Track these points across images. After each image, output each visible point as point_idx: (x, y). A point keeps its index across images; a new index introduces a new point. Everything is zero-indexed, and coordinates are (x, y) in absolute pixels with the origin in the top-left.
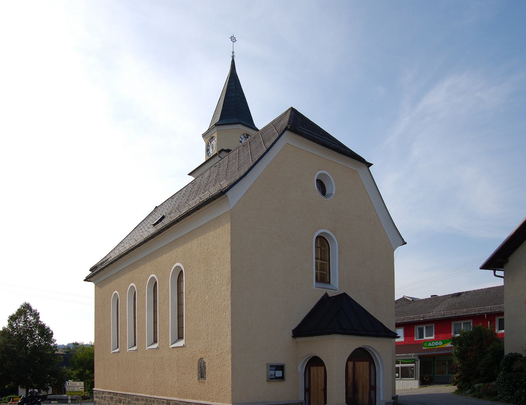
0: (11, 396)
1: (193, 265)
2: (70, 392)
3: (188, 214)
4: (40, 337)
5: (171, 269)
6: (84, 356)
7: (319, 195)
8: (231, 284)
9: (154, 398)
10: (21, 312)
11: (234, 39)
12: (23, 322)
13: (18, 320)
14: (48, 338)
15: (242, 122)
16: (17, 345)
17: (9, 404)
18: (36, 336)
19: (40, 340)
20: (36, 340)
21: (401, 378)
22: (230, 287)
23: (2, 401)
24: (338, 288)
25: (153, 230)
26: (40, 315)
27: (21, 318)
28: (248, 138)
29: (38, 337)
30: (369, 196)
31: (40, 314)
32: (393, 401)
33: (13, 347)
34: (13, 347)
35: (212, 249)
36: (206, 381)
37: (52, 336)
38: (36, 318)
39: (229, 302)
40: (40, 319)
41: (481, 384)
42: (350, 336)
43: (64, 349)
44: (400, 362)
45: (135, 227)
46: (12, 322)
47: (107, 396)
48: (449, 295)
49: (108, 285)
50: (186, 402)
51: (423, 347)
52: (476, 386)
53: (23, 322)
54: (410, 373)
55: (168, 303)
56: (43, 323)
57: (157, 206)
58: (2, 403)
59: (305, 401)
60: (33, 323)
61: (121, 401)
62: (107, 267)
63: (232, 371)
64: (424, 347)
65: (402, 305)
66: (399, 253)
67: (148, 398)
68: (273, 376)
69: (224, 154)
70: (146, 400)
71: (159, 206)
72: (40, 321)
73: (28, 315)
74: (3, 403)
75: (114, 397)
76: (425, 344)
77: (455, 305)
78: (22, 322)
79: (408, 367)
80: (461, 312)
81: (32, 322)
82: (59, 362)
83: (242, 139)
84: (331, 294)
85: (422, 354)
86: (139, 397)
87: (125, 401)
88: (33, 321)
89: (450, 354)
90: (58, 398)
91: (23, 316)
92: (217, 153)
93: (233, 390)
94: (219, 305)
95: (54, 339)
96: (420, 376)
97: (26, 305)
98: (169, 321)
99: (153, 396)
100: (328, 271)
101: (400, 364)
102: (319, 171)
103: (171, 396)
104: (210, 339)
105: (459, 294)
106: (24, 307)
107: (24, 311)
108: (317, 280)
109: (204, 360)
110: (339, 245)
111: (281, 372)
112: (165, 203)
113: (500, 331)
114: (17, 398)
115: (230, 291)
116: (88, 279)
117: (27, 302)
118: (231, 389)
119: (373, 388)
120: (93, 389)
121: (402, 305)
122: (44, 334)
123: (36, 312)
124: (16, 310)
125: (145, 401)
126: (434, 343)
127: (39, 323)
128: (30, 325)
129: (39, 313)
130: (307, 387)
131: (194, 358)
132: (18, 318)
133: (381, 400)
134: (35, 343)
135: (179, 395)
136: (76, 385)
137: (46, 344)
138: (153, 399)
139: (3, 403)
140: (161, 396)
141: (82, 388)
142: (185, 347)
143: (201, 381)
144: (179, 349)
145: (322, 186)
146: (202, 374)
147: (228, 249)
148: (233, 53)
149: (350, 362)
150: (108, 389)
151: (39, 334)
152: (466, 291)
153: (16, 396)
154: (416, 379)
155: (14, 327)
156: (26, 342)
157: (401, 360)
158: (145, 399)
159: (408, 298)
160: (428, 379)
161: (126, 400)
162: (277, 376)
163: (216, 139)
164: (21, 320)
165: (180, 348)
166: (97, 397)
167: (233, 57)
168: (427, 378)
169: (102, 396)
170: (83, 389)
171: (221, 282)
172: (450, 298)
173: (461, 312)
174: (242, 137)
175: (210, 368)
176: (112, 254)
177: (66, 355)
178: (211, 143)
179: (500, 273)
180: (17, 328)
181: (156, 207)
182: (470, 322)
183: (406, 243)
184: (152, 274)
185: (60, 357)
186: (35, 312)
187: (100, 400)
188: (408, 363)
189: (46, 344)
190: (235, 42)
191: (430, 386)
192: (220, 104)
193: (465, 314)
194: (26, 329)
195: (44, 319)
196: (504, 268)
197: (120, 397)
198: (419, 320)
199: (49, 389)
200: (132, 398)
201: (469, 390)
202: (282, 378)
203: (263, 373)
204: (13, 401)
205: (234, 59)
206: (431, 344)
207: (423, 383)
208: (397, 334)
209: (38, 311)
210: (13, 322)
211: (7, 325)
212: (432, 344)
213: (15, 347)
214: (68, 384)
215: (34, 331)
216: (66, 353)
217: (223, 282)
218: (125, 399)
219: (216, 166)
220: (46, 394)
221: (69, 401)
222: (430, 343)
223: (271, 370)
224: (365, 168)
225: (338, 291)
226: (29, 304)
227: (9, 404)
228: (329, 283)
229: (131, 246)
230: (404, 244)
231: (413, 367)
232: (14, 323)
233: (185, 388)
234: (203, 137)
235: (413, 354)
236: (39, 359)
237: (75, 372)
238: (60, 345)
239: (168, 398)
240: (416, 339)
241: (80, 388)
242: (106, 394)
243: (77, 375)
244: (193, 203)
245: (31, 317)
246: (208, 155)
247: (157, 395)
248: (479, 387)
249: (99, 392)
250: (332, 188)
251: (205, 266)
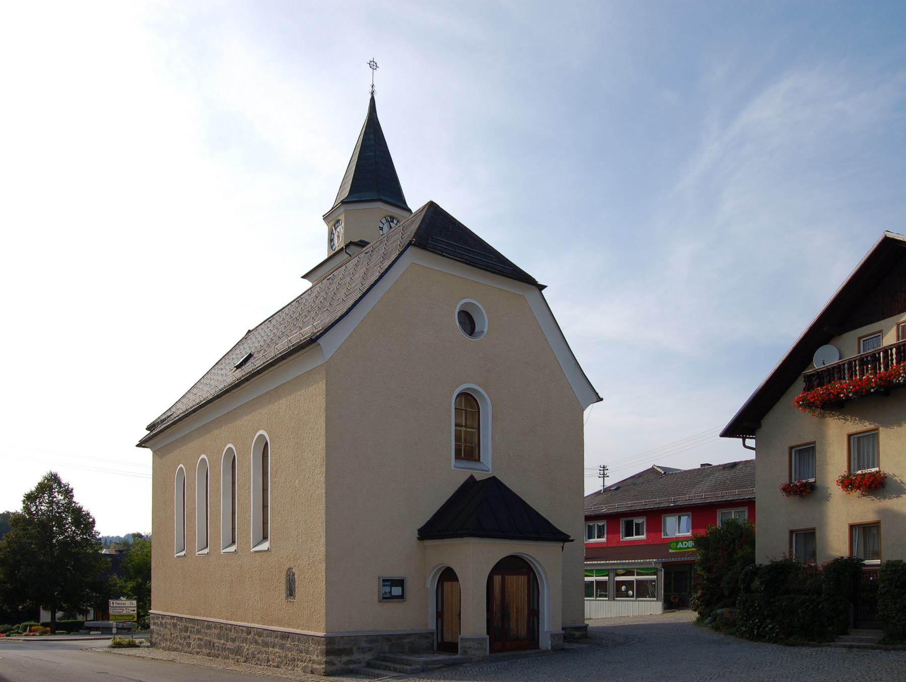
0: (27, 623)
1: (280, 436)
2: (115, 616)
3: (272, 364)
4: (74, 528)
5: (253, 438)
6: (144, 559)
7: (463, 334)
8: (326, 466)
9: (231, 624)
10: (44, 488)
11: (374, 64)
12: (47, 503)
13: (40, 500)
14: (87, 530)
15: (383, 198)
16: (37, 541)
17: (25, 635)
18: (67, 526)
19: (74, 532)
20: (68, 533)
21: (637, 597)
22: (324, 470)
23: (13, 630)
24: (491, 468)
25: (233, 376)
26: (75, 493)
27: (44, 497)
28: (393, 222)
29: (71, 528)
30: (542, 331)
31: (73, 491)
32: (563, 632)
33: (31, 543)
34: (31, 543)
35: (303, 414)
36: (295, 600)
37: (94, 527)
38: (67, 497)
39: (323, 491)
40: (75, 499)
41: (724, 610)
42: (495, 539)
43: (118, 544)
45: (216, 362)
46: (29, 503)
47: (169, 623)
48: (720, 465)
49: (171, 455)
50: (270, 630)
52: (719, 611)
53: (47, 503)
54: (650, 589)
55: (249, 488)
56: (78, 505)
57: (251, 329)
58: (12, 633)
59: (436, 630)
60: (63, 505)
61: (188, 630)
62: (168, 428)
63: (326, 587)
64: (672, 549)
65: (648, 481)
66: (592, 415)
67: (222, 625)
68: (389, 594)
69: (353, 250)
70: (221, 627)
71: (253, 330)
72: (74, 502)
73: (55, 492)
74: (14, 633)
75: (178, 623)
76: (673, 545)
77: (724, 482)
78: (45, 503)
79: (647, 581)
80: (731, 495)
81: (61, 503)
82: (104, 568)
83: (384, 224)
84: (480, 476)
85: (667, 560)
86: (211, 623)
87: (193, 630)
88: (63, 502)
89: (691, 564)
90: (103, 626)
91: (47, 494)
92: (343, 247)
93: (327, 615)
94: (312, 494)
95: (97, 530)
96: (665, 596)
97: (52, 475)
98: (250, 512)
99: (228, 621)
100: (477, 444)
101: (636, 575)
102: (462, 299)
103: (252, 622)
104: (300, 541)
105: (734, 465)
106: (48, 480)
107: (49, 485)
108: (458, 456)
109: (293, 570)
110: (492, 406)
111: (400, 588)
112: (262, 326)
113: (589, 540)
114: (38, 625)
115: (324, 475)
116: (142, 444)
117: (54, 471)
118: (324, 611)
119: (534, 613)
120: (150, 611)
121: (648, 481)
122: (81, 523)
123: (68, 488)
124: (36, 484)
125: (219, 630)
126: (686, 542)
127: (73, 505)
128: (59, 508)
129: (72, 489)
130: (440, 610)
131: (281, 567)
132: (39, 498)
133: (545, 630)
134: (66, 537)
135: (262, 621)
136: (124, 606)
137: (82, 539)
138: (229, 626)
139: (15, 635)
140: (241, 622)
141: (134, 611)
142: (270, 551)
143: (289, 600)
144: (262, 553)
145: (468, 321)
146: (291, 592)
147: (322, 417)
148: (372, 87)
149: (497, 576)
150: (169, 612)
151: (72, 523)
152: (746, 460)
153: (36, 624)
154: (658, 599)
155: (32, 512)
156: (52, 535)
157: (637, 569)
158: (219, 626)
159: (659, 469)
160: (677, 600)
161: (194, 628)
162: (393, 594)
163: (343, 224)
164: (43, 501)
165: (265, 553)
166: (154, 624)
167: (372, 93)
168: (675, 598)
169: (161, 622)
170: (135, 612)
171: (314, 461)
172: (719, 470)
173: (731, 495)
174: (384, 221)
175: (300, 582)
176: (179, 405)
177: (117, 556)
178: (336, 229)
179: (751, 442)
180: (37, 512)
181: (249, 331)
182: (745, 511)
183: (602, 400)
184: (229, 443)
185: (106, 560)
186: (67, 487)
187: (158, 629)
188: (647, 574)
189: (82, 539)
190: (375, 69)
191: (678, 611)
192: (352, 167)
193: (737, 498)
194: (52, 515)
195: (81, 499)
196: (756, 434)
197: (187, 623)
198: (667, 506)
199: (89, 611)
200: (201, 625)
201: (709, 618)
202: (402, 597)
203: (373, 589)
204: (31, 631)
205: (375, 96)
206: (681, 545)
207: (669, 605)
208: (570, 537)
209: (70, 487)
210: (31, 504)
211: (22, 508)
212: (684, 544)
213: (34, 544)
214: (113, 603)
215: (65, 519)
216: (118, 553)
217: (317, 462)
218: (193, 626)
219: (329, 279)
220: (85, 620)
221: (114, 631)
222: (680, 543)
223: (383, 586)
224: (537, 291)
225: (490, 472)
226: (56, 475)
227: (25, 635)
228: (479, 460)
229: (202, 399)
230: (598, 401)
231: (654, 581)
232: (32, 505)
233: (270, 611)
234: (324, 219)
235: (654, 560)
236: (73, 562)
237: (130, 584)
238: (113, 537)
239: (249, 624)
240: (664, 535)
242: (168, 619)
243: (133, 589)
244: (283, 346)
245: (60, 496)
246: (332, 248)
247: (234, 621)
248: (722, 614)
249: (158, 616)
250: (483, 323)
251: (296, 437)
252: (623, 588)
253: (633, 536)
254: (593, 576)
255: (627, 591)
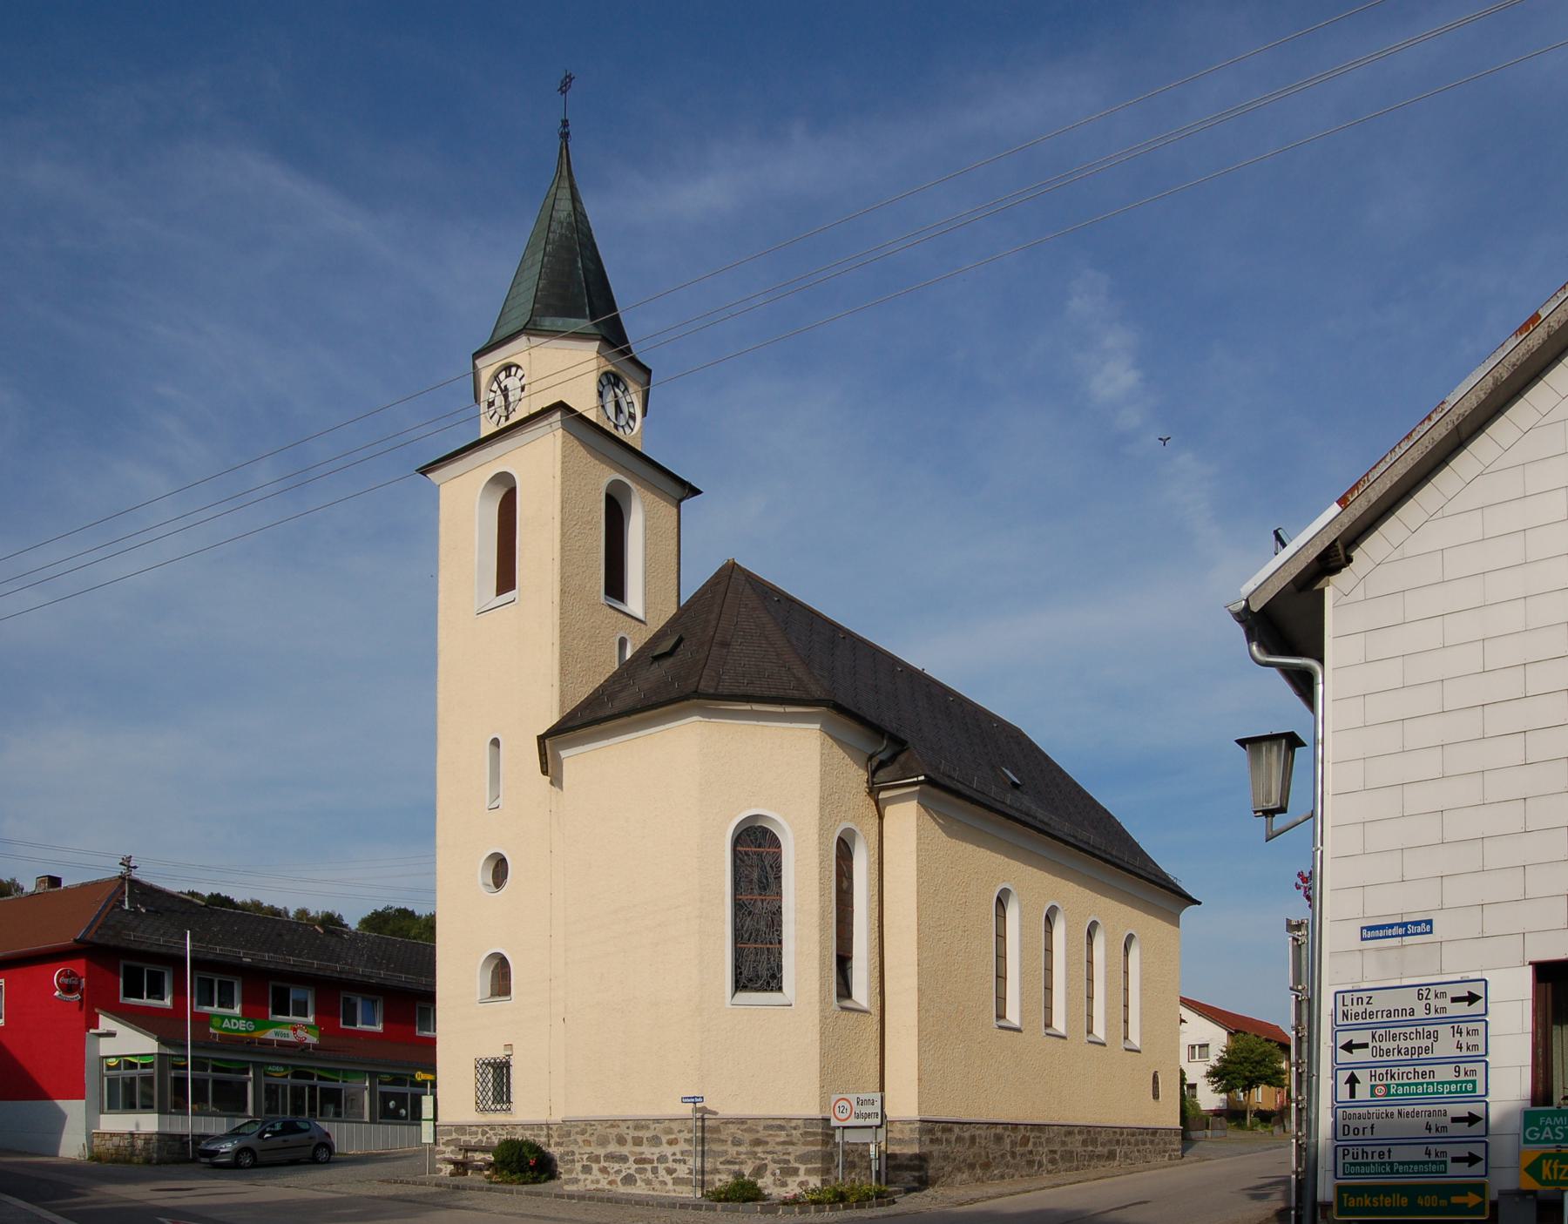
44: (210, 1065)
47: (984, 1136)
51: (211, 1029)
113: (200, 1007)
157: (214, 1059)
222: (226, 1020)
241: (1454, 1000)
252: (392, 1104)
253: (289, 1015)
254: (338, 1081)
255: (397, 1108)
